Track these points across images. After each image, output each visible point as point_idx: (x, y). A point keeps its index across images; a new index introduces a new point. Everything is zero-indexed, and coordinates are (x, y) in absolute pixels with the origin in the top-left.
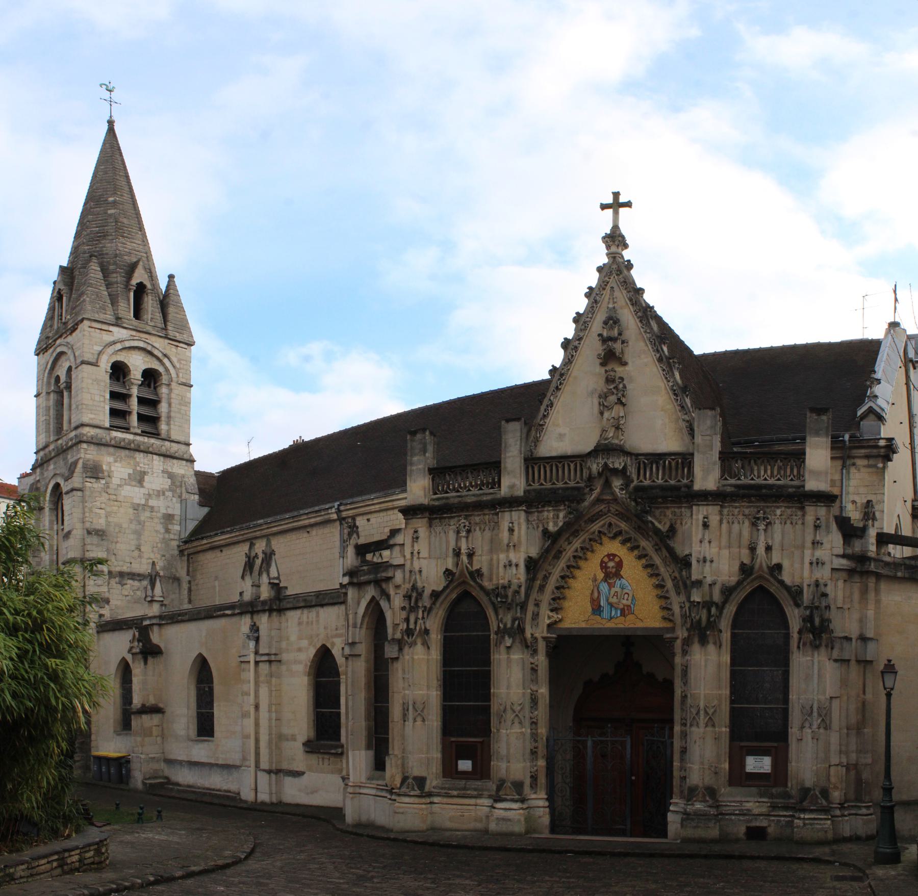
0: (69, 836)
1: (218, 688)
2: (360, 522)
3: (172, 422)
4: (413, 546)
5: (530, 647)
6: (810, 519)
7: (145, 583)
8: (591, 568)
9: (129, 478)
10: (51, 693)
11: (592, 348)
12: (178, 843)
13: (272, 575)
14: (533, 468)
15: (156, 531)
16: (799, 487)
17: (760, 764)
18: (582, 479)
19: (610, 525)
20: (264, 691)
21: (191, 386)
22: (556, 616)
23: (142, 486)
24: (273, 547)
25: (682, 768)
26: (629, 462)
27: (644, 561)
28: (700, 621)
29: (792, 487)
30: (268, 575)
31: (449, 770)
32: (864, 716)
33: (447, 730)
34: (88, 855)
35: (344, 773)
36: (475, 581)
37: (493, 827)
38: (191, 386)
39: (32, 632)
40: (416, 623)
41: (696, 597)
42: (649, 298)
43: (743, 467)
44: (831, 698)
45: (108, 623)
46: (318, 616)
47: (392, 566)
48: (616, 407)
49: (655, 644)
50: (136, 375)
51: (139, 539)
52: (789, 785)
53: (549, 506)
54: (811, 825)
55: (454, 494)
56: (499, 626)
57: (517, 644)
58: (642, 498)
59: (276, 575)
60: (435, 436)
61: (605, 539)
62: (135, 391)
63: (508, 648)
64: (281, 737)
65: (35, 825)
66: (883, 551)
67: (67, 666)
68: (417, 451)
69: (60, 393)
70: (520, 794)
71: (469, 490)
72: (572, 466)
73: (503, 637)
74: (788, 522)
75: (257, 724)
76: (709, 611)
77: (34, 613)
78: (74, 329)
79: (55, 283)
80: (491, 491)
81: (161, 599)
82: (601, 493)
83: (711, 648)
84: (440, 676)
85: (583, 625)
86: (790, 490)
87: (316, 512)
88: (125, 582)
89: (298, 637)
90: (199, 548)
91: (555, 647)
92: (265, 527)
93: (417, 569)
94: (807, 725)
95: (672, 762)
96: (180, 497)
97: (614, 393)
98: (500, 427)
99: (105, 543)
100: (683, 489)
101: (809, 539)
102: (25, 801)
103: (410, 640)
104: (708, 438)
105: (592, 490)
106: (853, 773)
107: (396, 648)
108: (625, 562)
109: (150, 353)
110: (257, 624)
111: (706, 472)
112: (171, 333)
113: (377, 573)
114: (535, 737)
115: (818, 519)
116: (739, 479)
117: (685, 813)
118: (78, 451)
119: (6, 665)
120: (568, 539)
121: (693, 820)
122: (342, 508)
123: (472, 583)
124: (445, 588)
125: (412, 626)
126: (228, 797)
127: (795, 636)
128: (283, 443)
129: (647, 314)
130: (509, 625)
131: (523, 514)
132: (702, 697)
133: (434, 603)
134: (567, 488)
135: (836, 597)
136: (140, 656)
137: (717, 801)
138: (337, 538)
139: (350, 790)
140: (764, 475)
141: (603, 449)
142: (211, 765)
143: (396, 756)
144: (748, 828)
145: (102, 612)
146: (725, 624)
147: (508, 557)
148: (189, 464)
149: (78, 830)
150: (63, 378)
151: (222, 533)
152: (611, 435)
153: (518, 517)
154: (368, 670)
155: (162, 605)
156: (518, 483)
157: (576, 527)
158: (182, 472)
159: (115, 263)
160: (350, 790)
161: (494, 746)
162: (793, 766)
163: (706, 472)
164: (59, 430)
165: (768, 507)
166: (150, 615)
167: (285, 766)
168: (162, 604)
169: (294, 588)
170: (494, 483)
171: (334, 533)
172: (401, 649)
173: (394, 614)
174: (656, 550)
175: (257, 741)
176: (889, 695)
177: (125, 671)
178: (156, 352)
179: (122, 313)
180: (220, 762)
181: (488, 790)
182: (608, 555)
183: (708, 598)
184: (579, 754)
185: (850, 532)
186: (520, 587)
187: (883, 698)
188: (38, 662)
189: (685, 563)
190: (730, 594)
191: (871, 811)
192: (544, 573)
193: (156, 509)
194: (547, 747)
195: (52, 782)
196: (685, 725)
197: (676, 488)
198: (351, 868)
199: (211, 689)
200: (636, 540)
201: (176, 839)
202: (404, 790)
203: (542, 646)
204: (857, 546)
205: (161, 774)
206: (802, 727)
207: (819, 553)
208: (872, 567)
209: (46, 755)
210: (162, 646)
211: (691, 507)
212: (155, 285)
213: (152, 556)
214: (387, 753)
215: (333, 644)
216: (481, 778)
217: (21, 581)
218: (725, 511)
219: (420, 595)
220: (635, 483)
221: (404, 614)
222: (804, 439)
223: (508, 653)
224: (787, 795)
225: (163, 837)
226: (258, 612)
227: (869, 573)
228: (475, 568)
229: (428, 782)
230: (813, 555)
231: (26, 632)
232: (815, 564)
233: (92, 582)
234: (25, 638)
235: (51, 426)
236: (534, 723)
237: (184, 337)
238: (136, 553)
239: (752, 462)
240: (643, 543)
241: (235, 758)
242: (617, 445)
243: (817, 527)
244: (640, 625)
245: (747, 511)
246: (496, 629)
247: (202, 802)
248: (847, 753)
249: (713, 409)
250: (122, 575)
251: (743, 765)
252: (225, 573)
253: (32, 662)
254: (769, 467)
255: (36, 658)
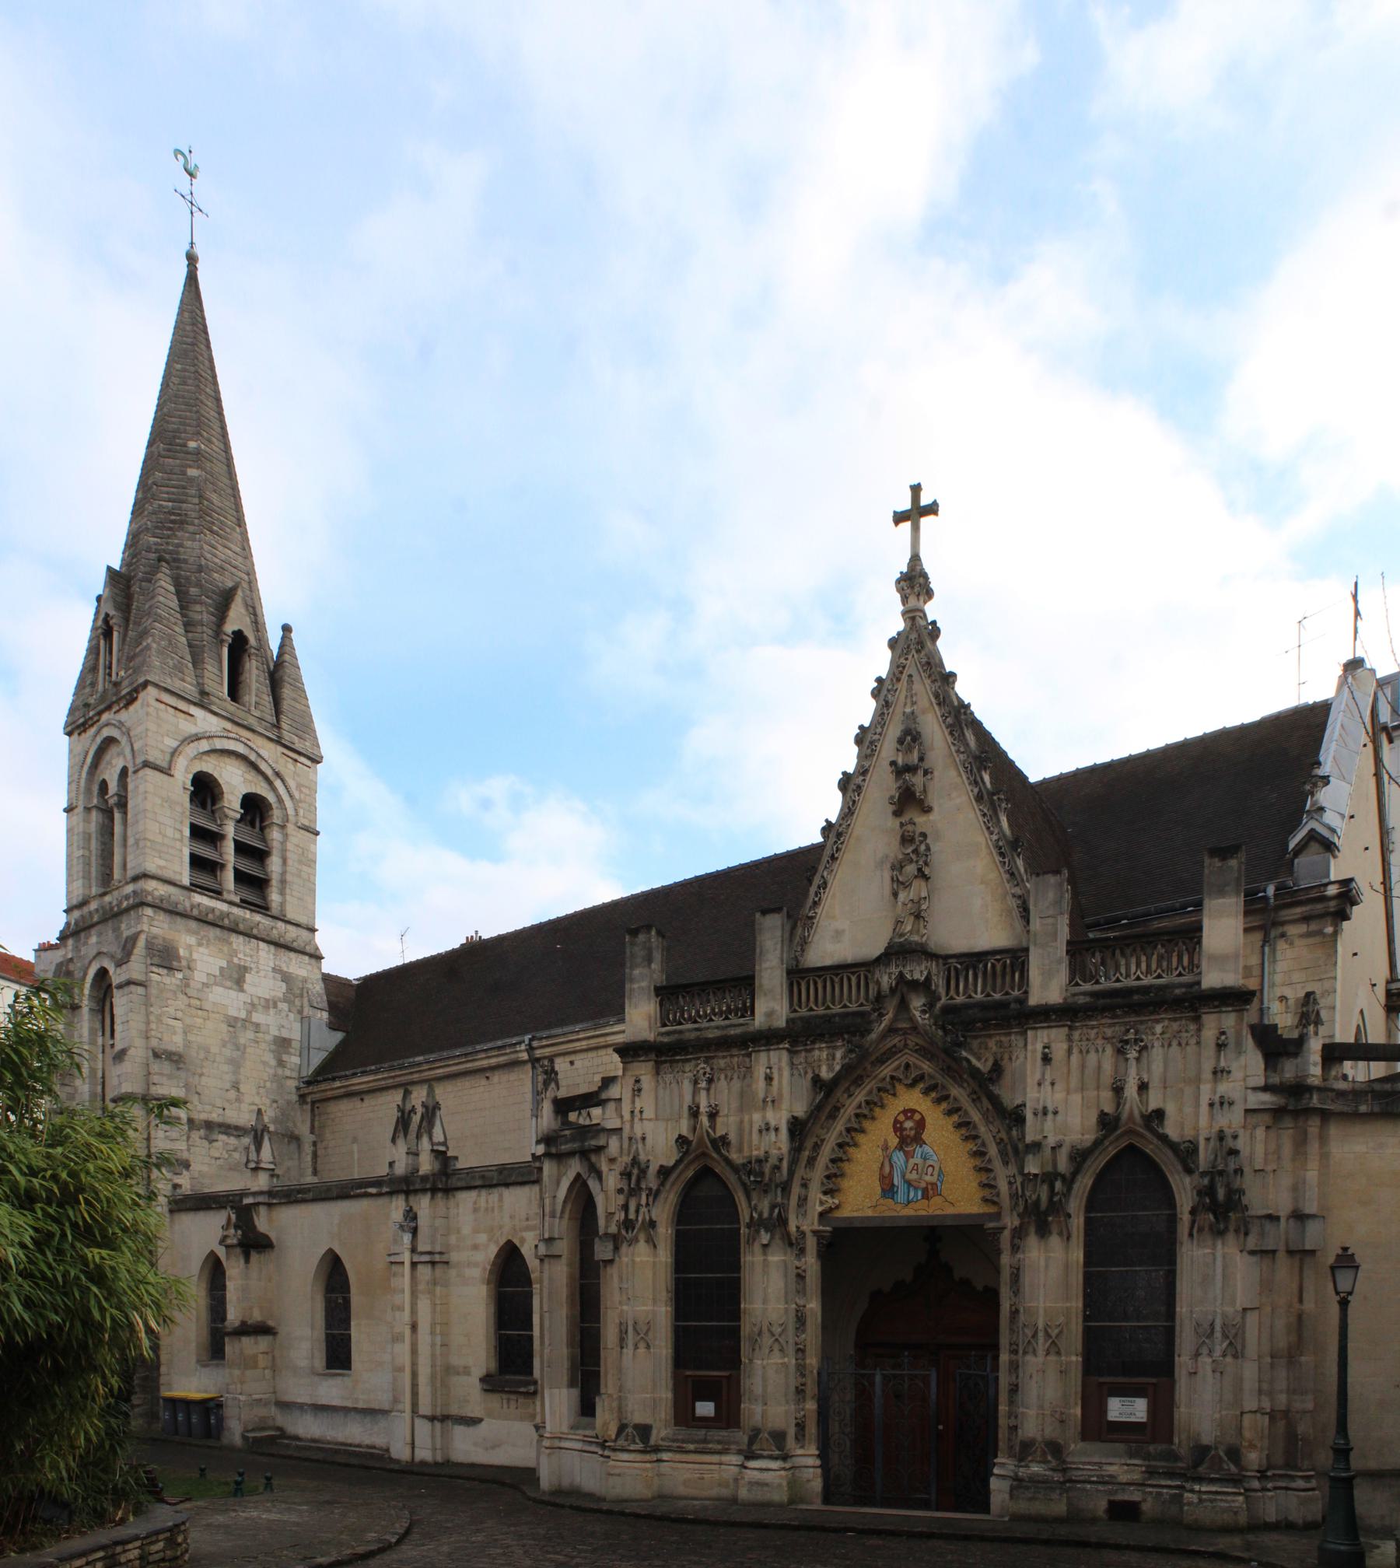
0: (123, 1521)
1: (356, 1299)
2: (561, 1065)
3: (288, 891)
4: (633, 1102)
5: (795, 1244)
6: (1209, 1034)
7: (247, 1140)
8: (881, 1131)
9: (222, 974)
10: (93, 1302)
11: (882, 787)
12: (298, 1524)
13: (435, 1140)
14: (799, 984)
15: (264, 1063)
16: (1190, 985)
17: (1129, 1410)
18: (867, 1000)
19: (907, 1066)
20: (424, 1305)
21: (317, 834)
22: (831, 1201)
23: (242, 990)
24: (438, 1098)
25: (1011, 1414)
26: (934, 970)
27: (955, 1118)
28: (1038, 1202)
29: (1181, 985)
30: (431, 1138)
31: (683, 1415)
32: (1300, 1337)
33: (680, 1360)
34: (154, 1548)
35: (538, 1420)
36: (719, 1152)
37: (743, 1493)
38: (317, 834)
39: (61, 1205)
40: (637, 1211)
41: (1032, 1167)
42: (963, 689)
43: (1103, 963)
44: (1244, 1310)
45: (187, 1198)
46: (501, 1199)
47: (604, 1130)
48: (916, 883)
49: (971, 1239)
50: (232, 802)
51: (236, 1072)
52: (1176, 1440)
53: (821, 1041)
54: (1209, 1501)
55: (690, 1026)
56: (752, 1217)
57: (777, 1241)
58: (952, 1024)
59: (442, 1139)
60: (663, 937)
61: (900, 1088)
62: (230, 830)
63: (765, 1246)
64: (449, 1370)
65: (65, 1505)
66: (1333, 1073)
67: (121, 1262)
68: (639, 960)
69: (108, 813)
70: (781, 1447)
71: (711, 1020)
72: (854, 979)
73: (758, 1232)
74: (1175, 1043)
75: (414, 1352)
76: (1052, 1187)
77: (64, 1175)
78: (131, 700)
79: (99, 599)
80: (742, 1020)
81: (272, 1166)
82: (895, 1020)
83: (1055, 1241)
84: (671, 1285)
85: (870, 1213)
86: (1177, 991)
87: (499, 1048)
88: (215, 1137)
89: (476, 1228)
90: (329, 1094)
91: (830, 1245)
92: (425, 1067)
93: (639, 1135)
94: (1205, 1351)
95: (997, 1406)
96: (300, 1012)
97: (913, 860)
98: (753, 922)
99: (183, 1074)
100: (1013, 1006)
101: (1208, 1067)
102: (47, 1470)
103: (630, 1235)
104: (1050, 920)
105: (881, 1015)
106: (1281, 1425)
107: (611, 1246)
108: (928, 1121)
109: (254, 766)
110: (415, 1209)
111: (1048, 975)
112: (287, 736)
113: (583, 1140)
114: (801, 1369)
115: (1223, 1033)
116: (1098, 982)
117: (1016, 1478)
118: (139, 918)
119: (12, 1254)
120: (848, 1089)
121: (1027, 1488)
122: (535, 1044)
123: (715, 1155)
124: (678, 1162)
125: (632, 1216)
126: (372, 1454)
127: (1185, 1217)
128: (450, 940)
129: (960, 718)
130: (766, 1215)
131: (785, 1055)
132: (1041, 1312)
133: (662, 1184)
134: (847, 1015)
135: (1252, 1154)
136: (238, 1250)
137: (1064, 1462)
138: (528, 1087)
139: (546, 1443)
140: (1136, 972)
141: (898, 951)
142: (346, 1410)
143: (610, 1396)
144: (1111, 1502)
145: (178, 1180)
146: (1076, 1206)
147: (764, 1117)
148: (313, 961)
149: (138, 1511)
150: (113, 787)
151: (364, 1073)
152: (909, 928)
153: (777, 1059)
154: (571, 1277)
155: (272, 1176)
156: (777, 1007)
157: (859, 1072)
158: (302, 973)
159: (199, 585)
160: (546, 1443)
161: (745, 1383)
162: (1181, 1412)
163: (1048, 975)
164: (106, 877)
165: (1142, 1022)
166: (255, 1189)
167: (454, 1411)
168: (273, 1174)
169: (467, 1158)
170: (745, 1009)
171: (523, 1081)
172: (616, 1249)
173: (607, 1199)
174: (974, 1101)
175: (414, 1375)
176: (1344, 1304)
177: (215, 1271)
178: (263, 767)
179: (210, 686)
180: (360, 1405)
181: (737, 1443)
182: (905, 1112)
183: (1049, 1169)
184: (863, 1394)
185: (1275, 1047)
186: (781, 1160)
187: (1335, 1309)
188: (69, 1252)
189: (1017, 1117)
190: (1084, 1160)
191: (1313, 1483)
192: (815, 1139)
193: (263, 1028)
194: (819, 1383)
195: (94, 1439)
196: (1016, 1352)
197: (1002, 1005)
198: (548, 1552)
199: (347, 1302)
200: (943, 1087)
201: (294, 1518)
202: (621, 1442)
203: (811, 1243)
204: (1289, 1070)
205: (270, 1423)
206: (1197, 1354)
207: (1224, 1088)
208: (1315, 1101)
209: (85, 1397)
210: (273, 1236)
211: (1025, 1032)
212: (262, 641)
213: (257, 1100)
214: (598, 1392)
215: (523, 1241)
216: (728, 1426)
217: (41, 1122)
218: (1076, 1035)
219: (643, 1172)
220: (943, 1000)
221: (621, 1200)
222: (1199, 904)
223: (765, 1254)
224: (1173, 1456)
225: (273, 1516)
226: (416, 1191)
227: (1308, 1111)
228: (718, 1134)
229: (654, 1432)
230: (1214, 1092)
231: (49, 1204)
232: (1217, 1106)
233: (161, 1134)
234: (46, 1214)
235: (93, 869)
236: (801, 1351)
237: (309, 751)
238: (233, 1094)
239: (1118, 952)
240: (955, 1091)
241: (382, 1400)
242: (917, 943)
243: (1220, 1047)
244: (951, 1211)
245: (1109, 1032)
246: (747, 1220)
247: (333, 1463)
248: (1271, 1394)
249: (1057, 872)
250: (209, 1125)
251: (1103, 1410)
252: (366, 1132)
253: (60, 1252)
254: (1144, 958)
255: (67, 1246)
